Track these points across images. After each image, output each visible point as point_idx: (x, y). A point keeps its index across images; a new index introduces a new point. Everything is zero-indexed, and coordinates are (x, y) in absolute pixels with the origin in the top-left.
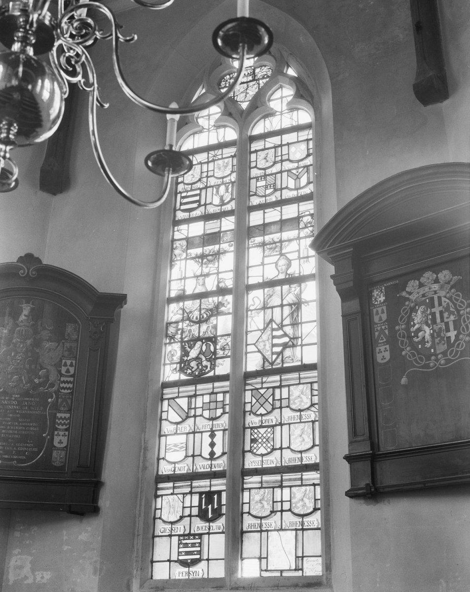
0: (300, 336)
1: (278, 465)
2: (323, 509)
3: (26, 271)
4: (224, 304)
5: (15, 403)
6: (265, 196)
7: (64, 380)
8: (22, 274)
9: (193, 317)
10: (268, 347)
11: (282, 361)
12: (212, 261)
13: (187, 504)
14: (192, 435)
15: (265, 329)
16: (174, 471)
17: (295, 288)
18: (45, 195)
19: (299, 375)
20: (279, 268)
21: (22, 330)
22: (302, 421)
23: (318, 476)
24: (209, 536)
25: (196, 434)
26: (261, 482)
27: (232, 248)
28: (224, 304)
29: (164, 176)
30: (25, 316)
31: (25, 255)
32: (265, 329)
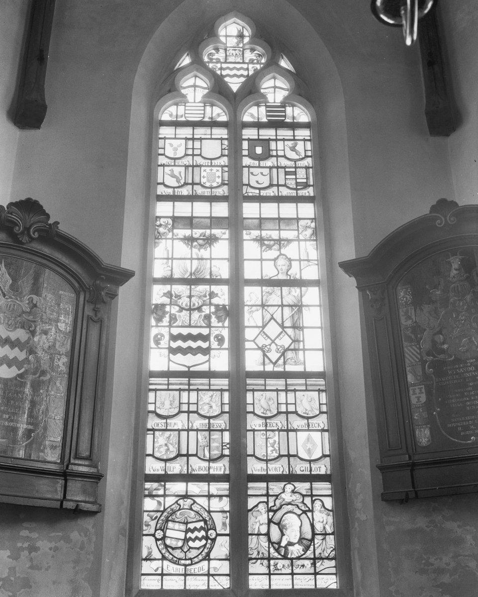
0: (301, 339)
3: (443, 219)
4: (217, 294)
5: (473, 368)
6: (211, 188)
8: (440, 224)
11: (285, 363)
12: (203, 245)
16: (311, 470)
17: (296, 291)
18: (439, 140)
19: (210, 381)
20: (279, 268)
21: (458, 286)
23: (227, 487)
27: (227, 236)
28: (217, 294)
30: (456, 270)
31: (437, 202)
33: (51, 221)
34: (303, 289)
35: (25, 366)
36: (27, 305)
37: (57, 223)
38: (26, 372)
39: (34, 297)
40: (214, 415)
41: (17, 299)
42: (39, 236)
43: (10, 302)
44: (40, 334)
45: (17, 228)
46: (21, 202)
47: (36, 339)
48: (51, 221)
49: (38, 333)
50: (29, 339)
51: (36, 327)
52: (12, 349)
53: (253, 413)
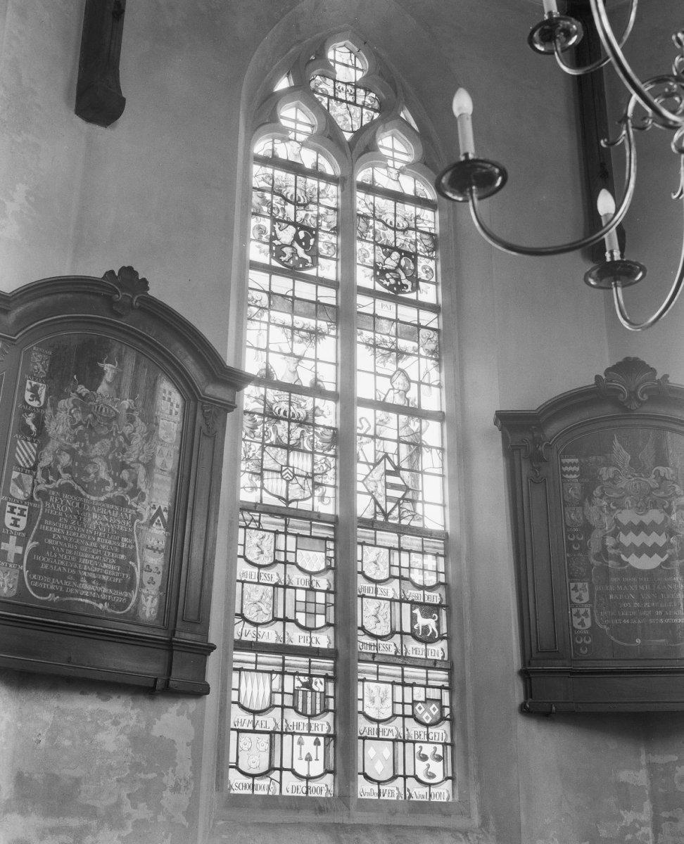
1: (279, 642)
2: (228, 702)
7: (643, 544)
9: (280, 410)
10: (381, 489)
13: (399, 699)
14: (281, 590)
15: (376, 464)
22: (260, 581)
24: (364, 741)
25: (288, 590)
26: (256, 663)
29: (612, 289)
32: (376, 464)
33: (659, 377)
34: (424, 422)
35: (668, 551)
36: (654, 481)
37: (666, 376)
38: (671, 558)
39: (660, 468)
40: (264, 563)
41: (641, 476)
42: (649, 397)
43: (634, 481)
44: (677, 510)
45: (622, 395)
46: (619, 364)
47: (674, 517)
48: (659, 377)
49: (674, 510)
50: (666, 519)
51: (670, 503)
52: (637, 535)
53: (244, 557)
